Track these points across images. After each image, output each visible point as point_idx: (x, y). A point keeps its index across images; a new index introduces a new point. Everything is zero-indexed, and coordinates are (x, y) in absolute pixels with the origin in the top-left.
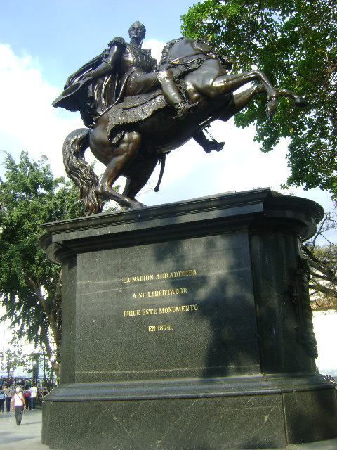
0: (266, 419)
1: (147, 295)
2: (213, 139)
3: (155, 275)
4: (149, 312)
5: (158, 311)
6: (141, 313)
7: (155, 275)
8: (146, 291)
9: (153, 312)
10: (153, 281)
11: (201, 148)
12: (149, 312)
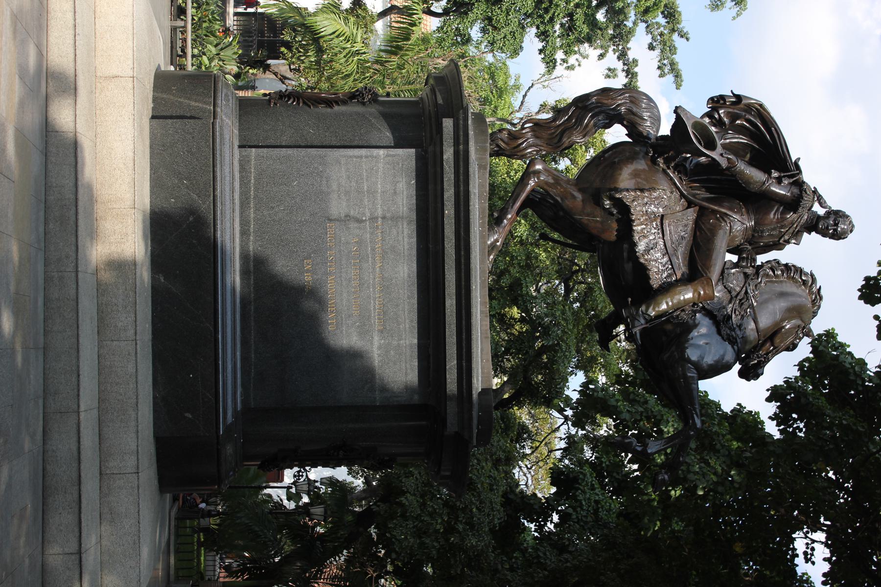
0: (187, 415)
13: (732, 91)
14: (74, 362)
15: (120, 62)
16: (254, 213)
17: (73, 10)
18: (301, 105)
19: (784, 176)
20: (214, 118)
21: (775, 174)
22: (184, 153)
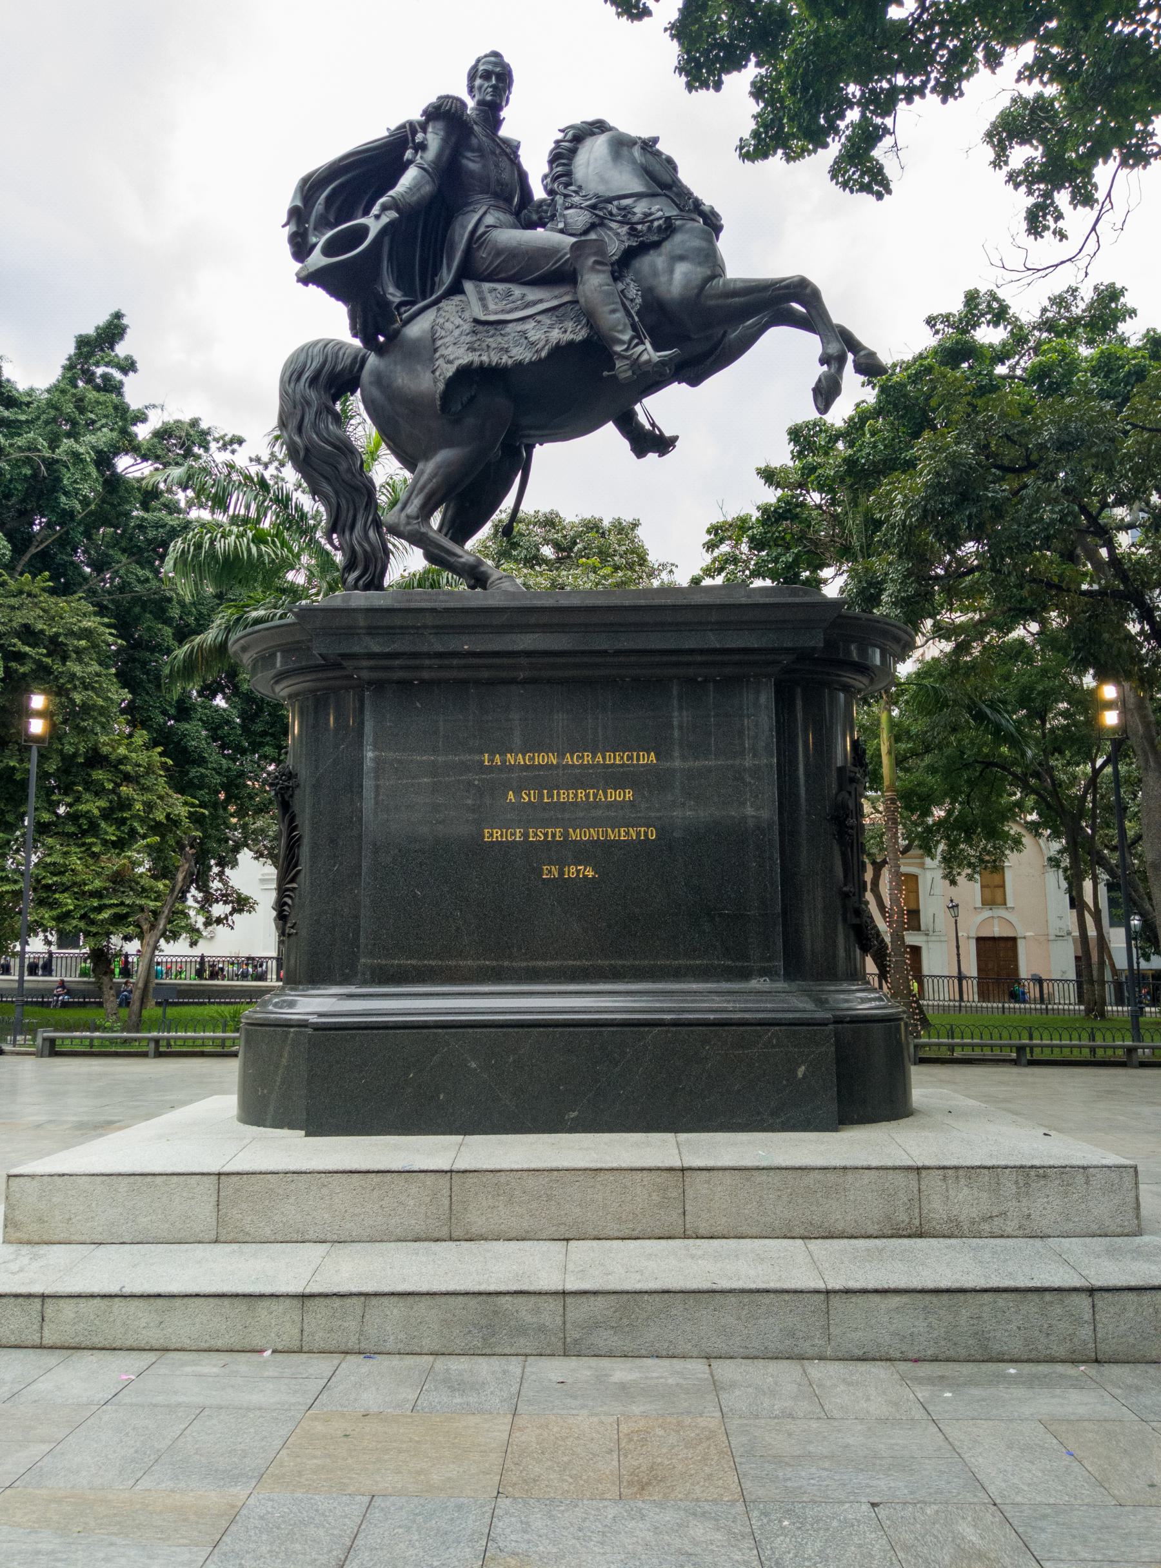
0: (800, 1074)
1: (541, 796)
2: (653, 425)
3: (561, 756)
4: (546, 835)
5: (566, 835)
6: (526, 835)
7: (561, 756)
8: (540, 787)
9: (554, 835)
10: (557, 766)
11: (626, 444)
12: (546, 835)
13: (284, 226)
14: (733, 1299)
15: (193, 1198)
16: (465, 959)
17: (75, 1300)
18: (295, 885)
19: (413, 140)
20: (306, 1026)
21: (408, 154)
22: (363, 1077)
